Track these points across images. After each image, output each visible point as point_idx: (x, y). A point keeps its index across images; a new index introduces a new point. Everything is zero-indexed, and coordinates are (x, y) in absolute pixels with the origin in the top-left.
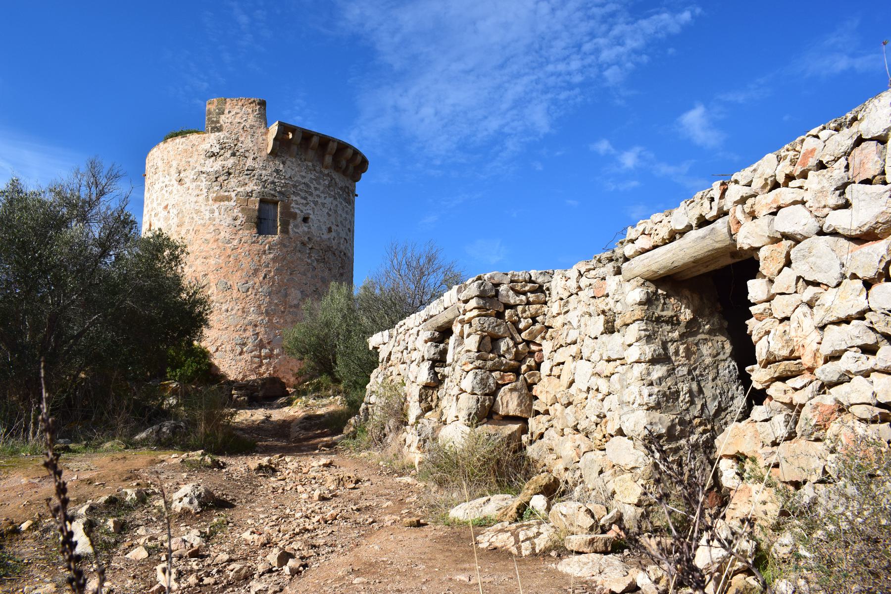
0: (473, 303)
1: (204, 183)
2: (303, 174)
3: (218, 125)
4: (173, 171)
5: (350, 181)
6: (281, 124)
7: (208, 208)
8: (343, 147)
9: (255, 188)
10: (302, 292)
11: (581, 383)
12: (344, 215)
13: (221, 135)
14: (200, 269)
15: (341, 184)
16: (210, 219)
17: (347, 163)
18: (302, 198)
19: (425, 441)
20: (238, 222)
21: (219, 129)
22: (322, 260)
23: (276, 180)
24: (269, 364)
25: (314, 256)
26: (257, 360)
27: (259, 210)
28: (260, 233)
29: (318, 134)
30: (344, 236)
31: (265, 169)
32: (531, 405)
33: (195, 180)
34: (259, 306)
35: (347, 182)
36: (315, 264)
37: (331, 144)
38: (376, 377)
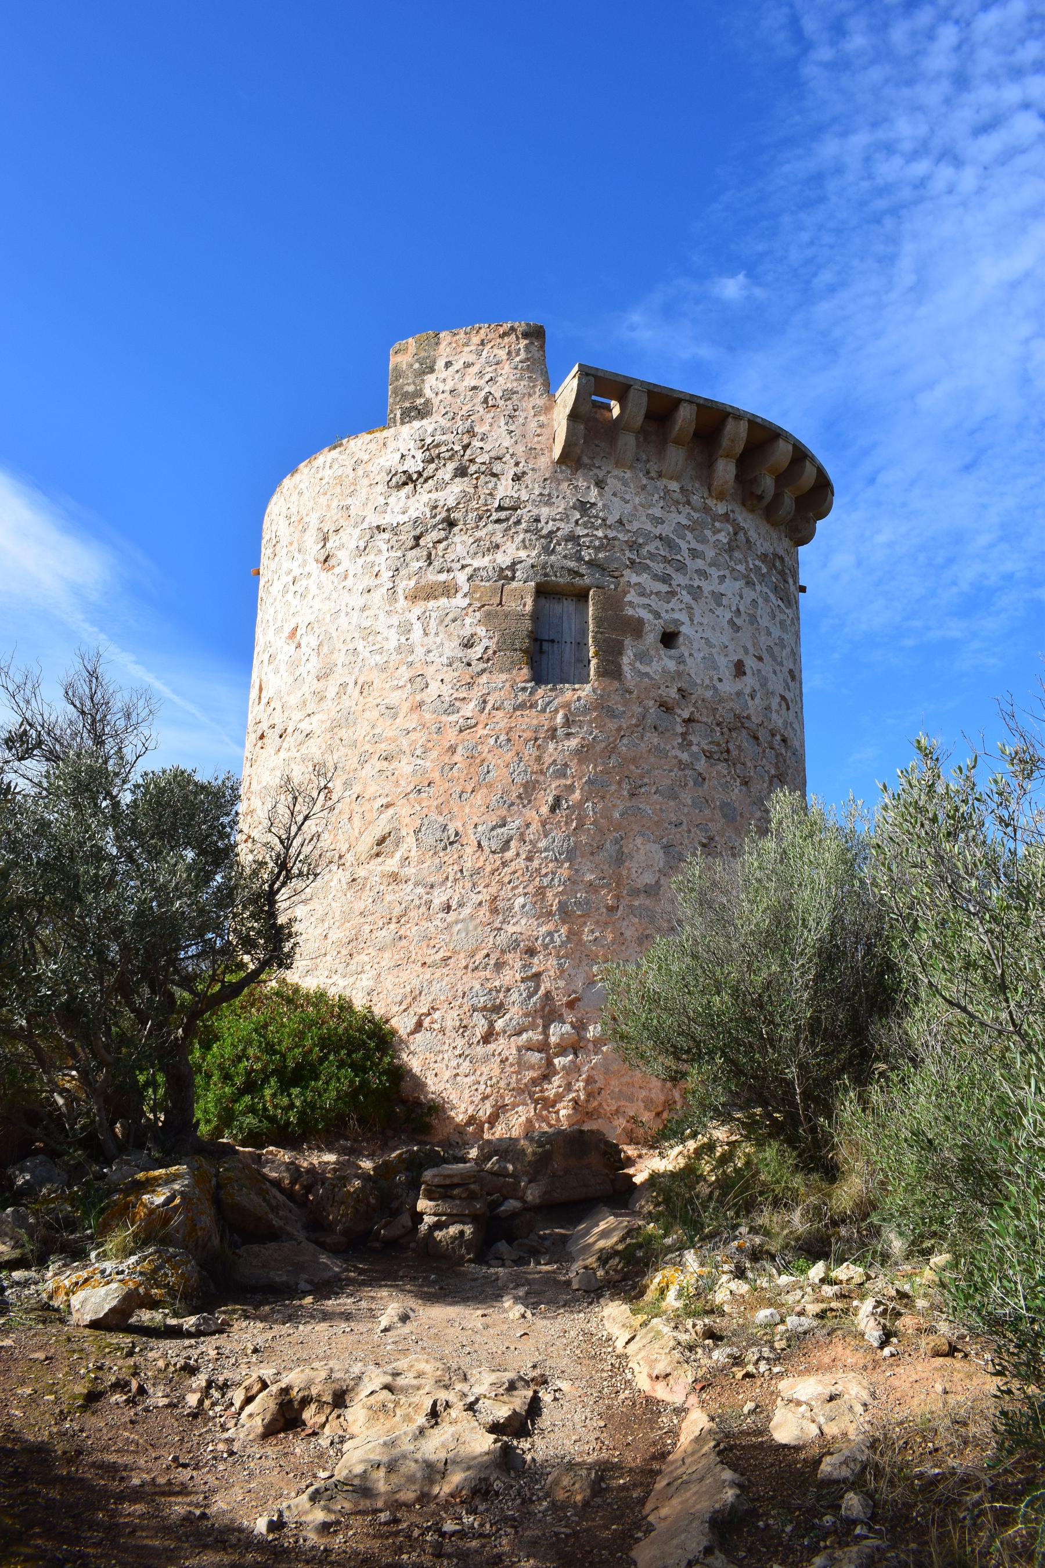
1: (383, 556)
2: (657, 512)
3: (420, 401)
5: (786, 543)
6: (585, 373)
7: (395, 620)
8: (764, 436)
9: (523, 554)
10: (667, 848)
12: (776, 632)
13: (427, 425)
14: (372, 789)
15: (763, 546)
16: (399, 649)
17: (776, 486)
18: (655, 577)
20: (477, 651)
21: (422, 412)
22: (724, 755)
23: (580, 531)
24: (573, 1070)
25: (699, 741)
26: (535, 1057)
27: (536, 616)
28: (538, 678)
29: (692, 400)
30: (780, 689)
31: (549, 503)
34: (541, 892)
35: (781, 546)
36: (702, 765)
37: (730, 425)
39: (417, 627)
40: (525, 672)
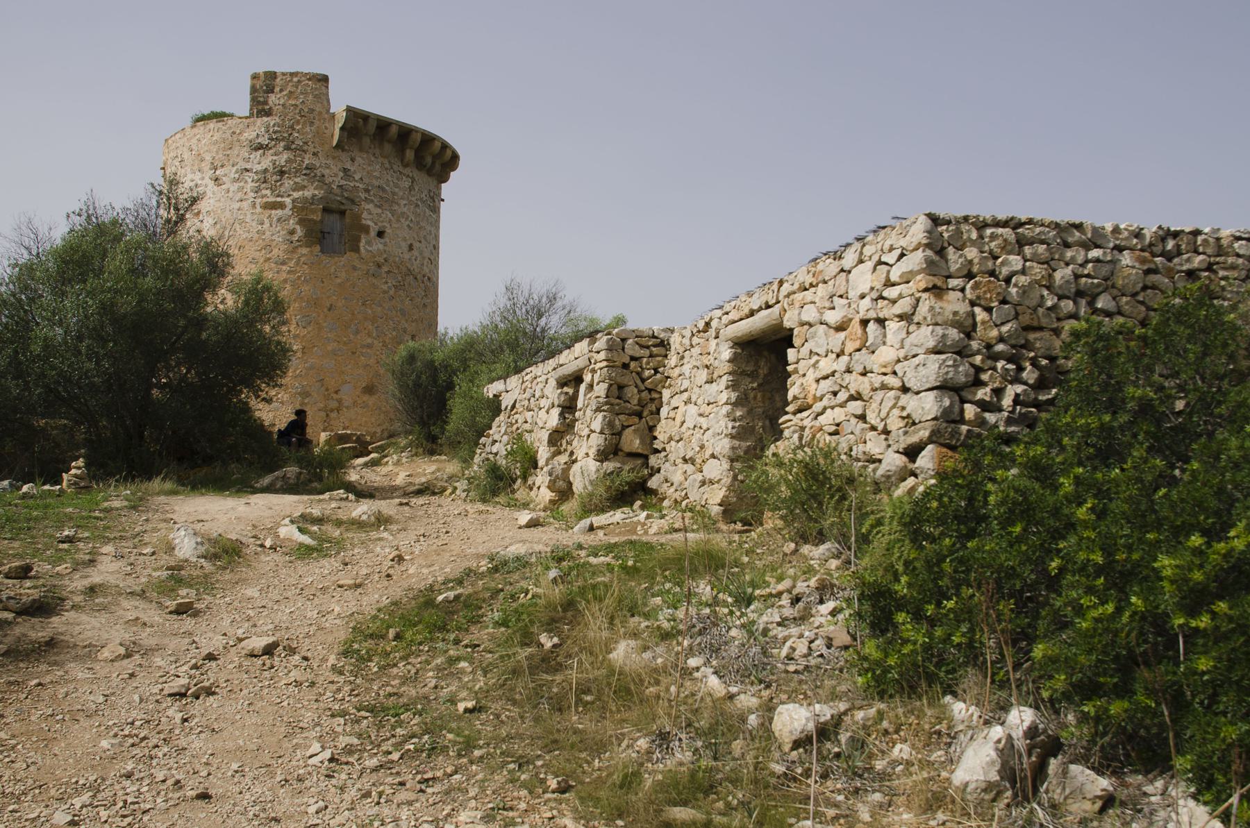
0: (602, 355)
4: (206, 166)
11: (689, 424)
16: (258, 232)
18: (376, 206)
19: (427, 780)
21: (268, 113)
25: (391, 282)
32: (652, 444)
33: (236, 180)
35: (432, 182)
37: (414, 135)
38: (498, 428)
39: (266, 221)
40: (318, 248)
